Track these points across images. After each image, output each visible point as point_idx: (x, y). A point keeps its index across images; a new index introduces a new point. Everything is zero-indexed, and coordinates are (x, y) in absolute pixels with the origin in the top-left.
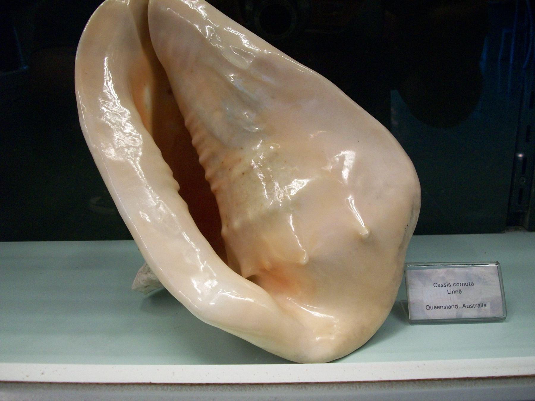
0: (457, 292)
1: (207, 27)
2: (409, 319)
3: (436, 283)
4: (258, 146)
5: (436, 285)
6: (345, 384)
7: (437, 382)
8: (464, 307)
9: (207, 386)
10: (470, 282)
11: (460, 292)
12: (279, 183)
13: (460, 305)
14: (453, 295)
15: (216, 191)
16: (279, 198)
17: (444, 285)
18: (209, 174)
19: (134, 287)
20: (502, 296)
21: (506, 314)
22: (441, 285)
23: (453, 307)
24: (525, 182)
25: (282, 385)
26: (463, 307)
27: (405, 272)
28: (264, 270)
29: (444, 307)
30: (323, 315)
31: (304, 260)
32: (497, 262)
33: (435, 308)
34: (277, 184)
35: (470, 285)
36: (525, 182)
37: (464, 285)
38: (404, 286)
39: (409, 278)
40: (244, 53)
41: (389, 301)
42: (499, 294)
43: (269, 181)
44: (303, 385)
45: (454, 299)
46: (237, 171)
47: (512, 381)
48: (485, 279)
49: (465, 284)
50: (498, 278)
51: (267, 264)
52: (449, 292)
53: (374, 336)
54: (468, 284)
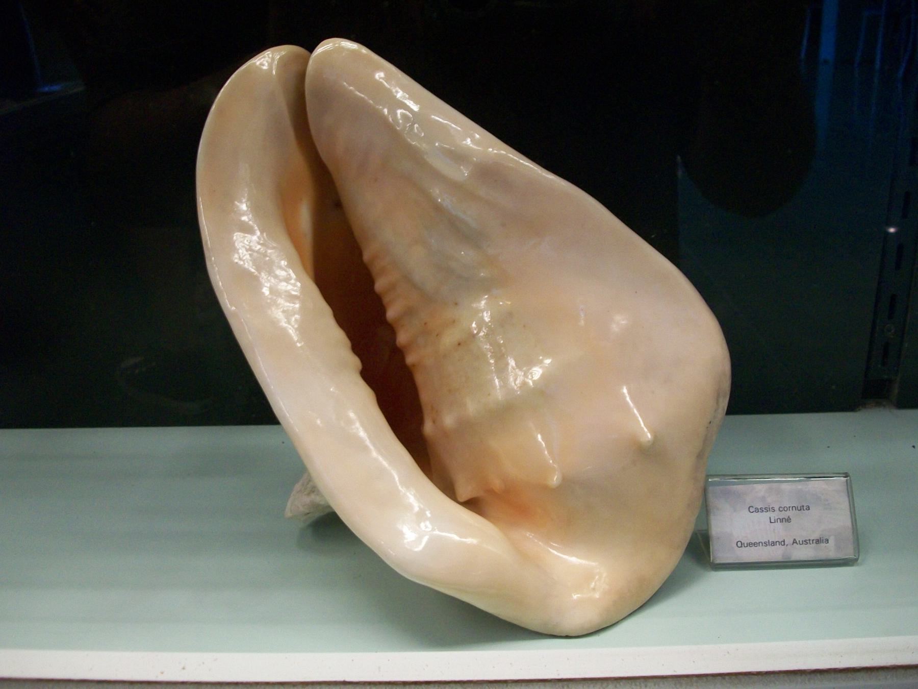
0: (784, 520)
1: (399, 112)
2: (711, 561)
3: (752, 507)
4: (483, 302)
5: (752, 510)
6: (624, 681)
7: (756, 677)
8: (795, 544)
9: (426, 686)
10: (804, 504)
11: (788, 520)
12: (515, 360)
13: (789, 541)
14: (778, 525)
15: (414, 366)
16: (515, 383)
17: (764, 510)
18: (402, 338)
19: (288, 514)
20: (853, 525)
21: (859, 552)
22: (760, 510)
23: (778, 543)
24: (893, 331)
25: (535, 684)
26: (794, 543)
27: (705, 491)
28: (491, 492)
29: (764, 543)
30: (583, 562)
31: (555, 480)
32: (846, 473)
33: (750, 545)
34: (512, 363)
35: (805, 509)
36: (893, 331)
37: (796, 509)
38: (705, 510)
39: (713, 500)
40: (459, 157)
41: (682, 537)
42: (849, 523)
43: (500, 357)
44: (565, 683)
45: (779, 531)
46: (449, 339)
47: (862, 674)
48: (827, 500)
49: (796, 508)
50: (847, 499)
51: (497, 484)
52: (772, 521)
53: (660, 588)
54: (802, 508)
